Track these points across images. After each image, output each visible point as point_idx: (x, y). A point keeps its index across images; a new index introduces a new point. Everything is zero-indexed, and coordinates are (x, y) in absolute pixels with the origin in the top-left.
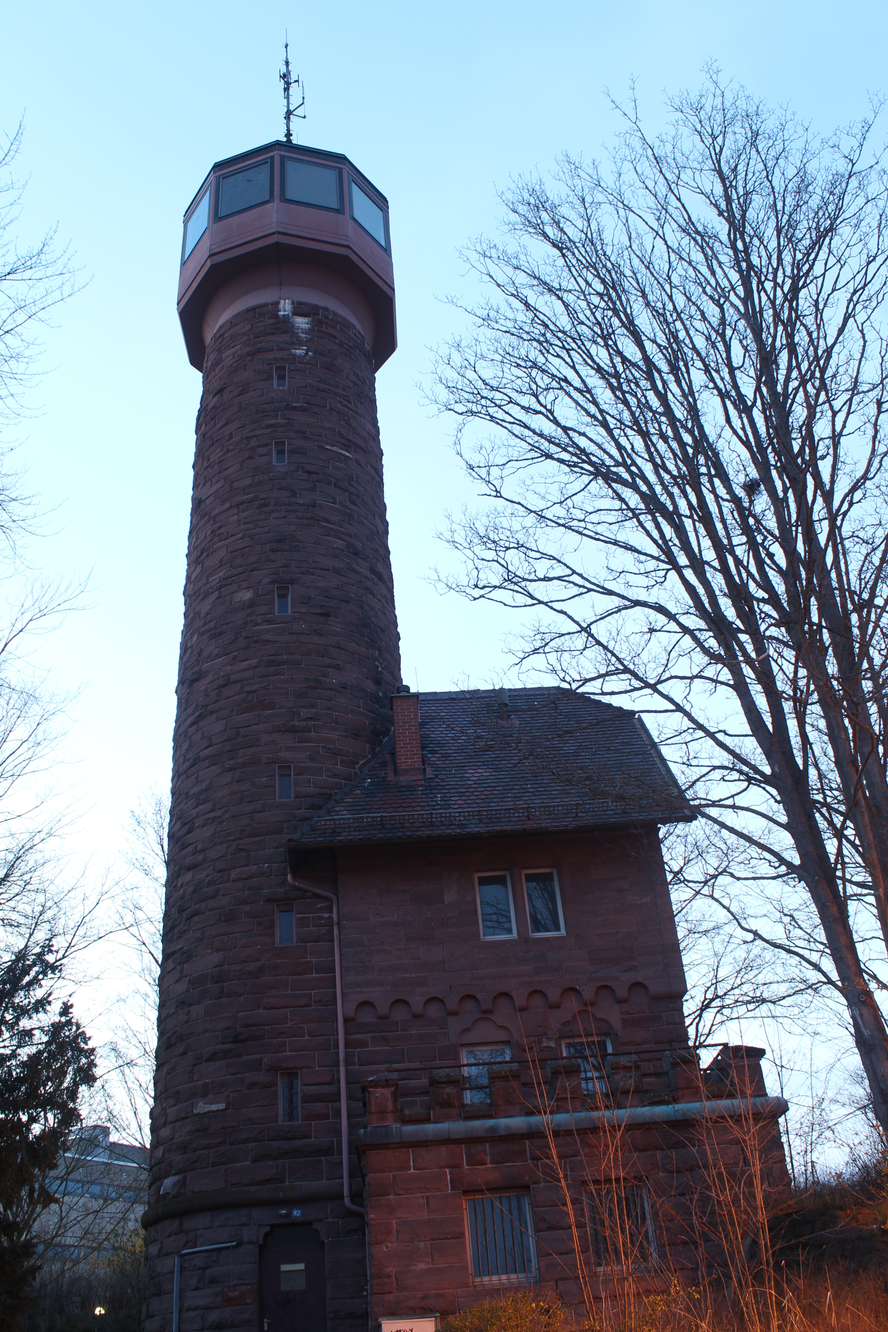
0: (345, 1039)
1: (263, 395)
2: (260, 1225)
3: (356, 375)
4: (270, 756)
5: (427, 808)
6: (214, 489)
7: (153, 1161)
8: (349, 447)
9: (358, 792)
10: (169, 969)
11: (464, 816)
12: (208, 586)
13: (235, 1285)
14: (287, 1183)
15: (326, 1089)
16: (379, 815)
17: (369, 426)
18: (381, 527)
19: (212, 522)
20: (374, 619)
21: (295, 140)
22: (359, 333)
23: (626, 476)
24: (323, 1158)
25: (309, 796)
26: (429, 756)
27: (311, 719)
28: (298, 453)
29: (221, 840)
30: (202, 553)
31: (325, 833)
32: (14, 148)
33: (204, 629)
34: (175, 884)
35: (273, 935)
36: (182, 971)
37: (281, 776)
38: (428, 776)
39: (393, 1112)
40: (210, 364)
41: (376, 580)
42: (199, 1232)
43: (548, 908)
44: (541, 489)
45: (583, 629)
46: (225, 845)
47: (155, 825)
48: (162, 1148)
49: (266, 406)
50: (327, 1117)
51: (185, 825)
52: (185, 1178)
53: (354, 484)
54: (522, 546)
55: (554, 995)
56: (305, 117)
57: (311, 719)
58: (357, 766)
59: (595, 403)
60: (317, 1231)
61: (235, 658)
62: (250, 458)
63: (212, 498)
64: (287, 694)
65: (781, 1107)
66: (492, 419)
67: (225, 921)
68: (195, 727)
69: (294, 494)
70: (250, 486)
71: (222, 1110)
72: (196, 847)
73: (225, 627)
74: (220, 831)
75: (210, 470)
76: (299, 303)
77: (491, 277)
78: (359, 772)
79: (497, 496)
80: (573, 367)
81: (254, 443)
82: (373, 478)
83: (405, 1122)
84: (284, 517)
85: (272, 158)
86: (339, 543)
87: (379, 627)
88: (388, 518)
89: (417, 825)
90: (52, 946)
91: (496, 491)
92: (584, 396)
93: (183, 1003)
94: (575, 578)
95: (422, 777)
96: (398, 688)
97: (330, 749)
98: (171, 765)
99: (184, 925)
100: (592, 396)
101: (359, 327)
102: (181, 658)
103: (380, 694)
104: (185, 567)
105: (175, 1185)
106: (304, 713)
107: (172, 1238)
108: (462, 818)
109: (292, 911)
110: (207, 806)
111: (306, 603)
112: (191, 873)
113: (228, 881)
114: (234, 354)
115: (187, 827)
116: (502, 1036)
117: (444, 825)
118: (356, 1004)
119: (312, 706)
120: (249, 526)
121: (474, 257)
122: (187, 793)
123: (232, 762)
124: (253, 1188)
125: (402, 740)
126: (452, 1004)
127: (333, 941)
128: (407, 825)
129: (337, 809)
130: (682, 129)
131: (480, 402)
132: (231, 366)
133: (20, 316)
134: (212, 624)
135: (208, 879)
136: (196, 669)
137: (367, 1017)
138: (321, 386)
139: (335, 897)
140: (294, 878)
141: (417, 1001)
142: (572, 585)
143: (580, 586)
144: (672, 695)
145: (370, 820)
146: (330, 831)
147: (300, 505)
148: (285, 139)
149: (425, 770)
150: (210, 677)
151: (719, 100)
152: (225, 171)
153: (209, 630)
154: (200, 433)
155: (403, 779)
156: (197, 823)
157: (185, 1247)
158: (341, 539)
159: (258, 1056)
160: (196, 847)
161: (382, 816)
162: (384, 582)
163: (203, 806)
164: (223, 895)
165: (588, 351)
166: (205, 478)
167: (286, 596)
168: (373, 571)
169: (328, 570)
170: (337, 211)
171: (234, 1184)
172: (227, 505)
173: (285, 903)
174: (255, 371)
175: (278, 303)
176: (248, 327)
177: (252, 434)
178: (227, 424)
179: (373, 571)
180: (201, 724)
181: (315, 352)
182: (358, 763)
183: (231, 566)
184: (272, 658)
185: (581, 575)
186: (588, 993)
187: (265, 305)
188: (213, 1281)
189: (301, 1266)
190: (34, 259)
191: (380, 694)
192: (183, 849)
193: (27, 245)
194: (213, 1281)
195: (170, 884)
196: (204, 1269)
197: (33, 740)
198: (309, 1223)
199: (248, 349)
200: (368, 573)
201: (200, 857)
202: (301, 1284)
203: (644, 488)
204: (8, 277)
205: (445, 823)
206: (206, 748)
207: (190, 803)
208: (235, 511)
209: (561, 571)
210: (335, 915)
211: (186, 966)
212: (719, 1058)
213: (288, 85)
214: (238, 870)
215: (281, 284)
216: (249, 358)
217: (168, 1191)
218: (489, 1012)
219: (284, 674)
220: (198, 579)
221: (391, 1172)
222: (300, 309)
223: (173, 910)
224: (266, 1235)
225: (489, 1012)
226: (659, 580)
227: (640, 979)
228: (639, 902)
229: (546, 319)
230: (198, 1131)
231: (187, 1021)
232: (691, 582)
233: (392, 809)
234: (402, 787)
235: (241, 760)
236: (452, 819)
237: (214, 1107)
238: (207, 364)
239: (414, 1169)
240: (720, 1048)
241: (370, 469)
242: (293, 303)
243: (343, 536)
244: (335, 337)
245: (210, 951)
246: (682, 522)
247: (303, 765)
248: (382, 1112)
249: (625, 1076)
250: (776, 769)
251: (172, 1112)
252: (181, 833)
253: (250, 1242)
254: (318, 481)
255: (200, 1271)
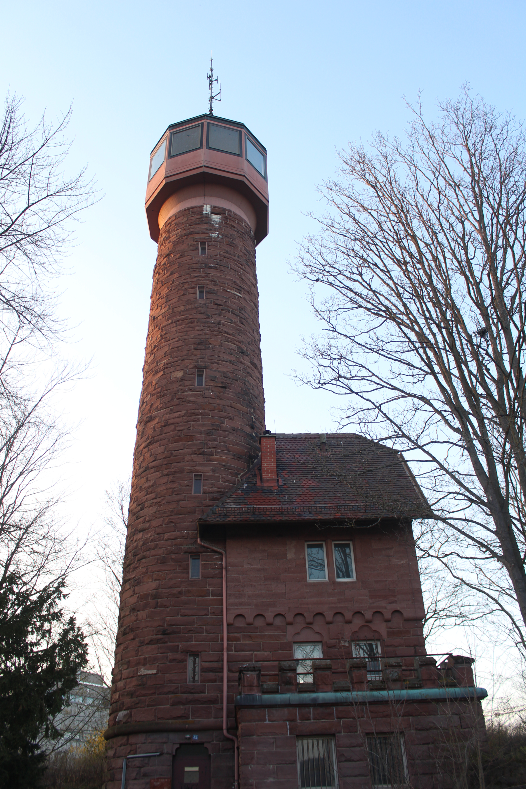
0: (228, 636)
1: (192, 259)
2: (174, 743)
3: (245, 249)
4: (190, 468)
5: (279, 503)
6: (163, 311)
7: (113, 700)
8: (241, 290)
9: (240, 491)
10: (127, 589)
11: (301, 509)
12: (157, 368)
13: (158, 779)
14: (190, 719)
15: (215, 665)
16: (252, 506)
17: (252, 279)
18: (257, 337)
19: (160, 331)
20: (251, 391)
21: (215, 114)
22: (248, 225)
23: (408, 322)
24: (212, 706)
25: (212, 493)
26: (281, 471)
27: (214, 448)
28: (212, 293)
29: (160, 516)
30: (154, 348)
31: (220, 515)
32: (66, 121)
33: (154, 392)
34: (132, 539)
35: (188, 573)
36: (134, 591)
37: (195, 480)
38: (280, 484)
39: (256, 686)
40: (162, 239)
41: (253, 368)
42: (138, 745)
43: (342, 559)
44: (354, 323)
45: (377, 407)
46: (162, 519)
47: (119, 499)
48: (118, 693)
49: (194, 265)
50: (215, 681)
51: (139, 505)
52: (131, 713)
53: (243, 312)
54: (344, 358)
55: (348, 615)
56: (220, 100)
57: (214, 448)
58: (239, 476)
59: (391, 278)
60: (206, 748)
61: (171, 410)
62: (184, 295)
63: (161, 317)
64: (201, 433)
65: (483, 694)
66: (331, 284)
67: (161, 563)
68: (146, 449)
69: (208, 317)
70: (184, 311)
71: (155, 674)
72: (145, 518)
73: (166, 392)
74: (159, 511)
75: (160, 300)
76: (215, 207)
77: (335, 202)
78: (240, 480)
79: (333, 331)
80: (380, 257)
81: (186, 286)
82: (253, 309)
83: (264, 692)
84: (202, 330)
85: (202, 124)
86: (233, 346)
87: (254, 395)
88: (260, 332)
89: (273, 513)
90: (65, 582)
91: (333, 328)
92: (386, 275)
93: (134, 609)
94: (374, 378)
95: (276, 484)
96: (264, 432)
97: (224, 466)
98: (132, 469)
99: (136, 564)
100: (390, 274)
101: (248, 222)
102: (140, 408)
103: (254, 434)
104: (144, 355)
105: (125, 716)
106: (210, 444)
107: (122, 747)
108: (299, 510)
109: (199, 559)
110: (153, 495)
111: (213, 380)
112: (141, 533)
113: (163, 540)
114: (177, 234)
115: (140, 507)
116: (318, 638)
117: (289, 514)
118: (234, 616)
119: (215, 440)
120: (182, 334)
121: (325, 191)
122: (141, 487)
123: (168, 470)
124: (171, 721)
125: (266, 462)
126: (290, 618)
127: (222, 578)
128: (268, 513)
129: (228, 501)
130: (448, 121)
131: (324, 273)
132: (175, 241)
133: (62, 215)
134: (159, 390)
135: (151, 538)
136: (149, 415)
137: (240, 623)
138: (226, 255)
139: (224, 552)
140: (201, 540)
141: (269, 616)
142: (373, 383)
143: (378, 384)
144: (431, 452)
145: (246, 509)
146: (223, 514)
147: (212, 323)
148: (208, 113)
149: (278, 480)
150: (156, 421)
151: (468, 106)
152: (176, 129)
153: (158, 393)
154: (155, 278)
155: (266, 485)
156: (146, 504)
157: (129, 753)
158: (234, 344)
159: (177, 643)
160: (145, 518)
161: (254, 507)
162: (258, 369)
163: (150, 495)
164: (160, 548)
165: (391, 249)
166: (157, 305)
167: (202, 376)
168: (252, 363)
169: (227, 362)
170: (238, 155)
171: (160, 718)
172: (170, 321)
173: (195, 555)
174: (188, 245)
175: (203, 206)
176: (185, 219)
177: (185, 281)
178: (171, 274)
179: (252, 363)
180: (151, 447)
181: (223, 235)
182: (240, 474)
183: (171, 357)
184: (193, 411)
185: (377, 377)
186: (368, 615)
187: (196, 207)
188: (145, 775)
189: (196, 769)
190: (73, 185)
191: (254, 434)
192: (137, 519)
193: (69, 177)
194: (145, 775)
195: (129, 538)
196: (140, 767)
197: (52, 450)
198: (203, 744)
199: (185, 232)
200: (249, 364)
201: (147, 525)
202: (196, 780)
203: (417, 329)
204: (57, 194)
205: (290, 513)
206: (153, 461)
207: (142, 493)
208: (175, 325)
209: (364, 373)
210: (224, 563)
211: (136, 588)
212: (447, 661)
213: (212, 81)
214: (169, 534)
215: (205, 195)
216: (185, 237)
217: (121, 719)
218: (311, 624)
219: (199, 421)
220: (152, 363)
221: (255, 722)
222: (215, 211)
223: (130, 554)
224: (177, 749)
225: (311, 624)
226: (420, 379)
227: (398, 609)
228: (399, 563)
229: (364, 228)
230: (140, 685)
231: (136, 620)
232: (444, 386)
233: (259, 503)
234: (265, 490)
235: (173, 470)
236: (294, 510)
237: (150, 672)
238: (161, 239)
239: (269, 720)
240: (448, 656)
241: (251, 303)
242: (211, 207)
243: (235, 342)
244: (234, 227)
245: (151, 580)
246: (440, 353)
247: (208, 474)
248: (251, 686)
249: (393, 671)
250: (490, 499)
251: (125, 673)
252: (136, 510)
253: (168, 753)
254: (222, 310)
255: (138, 769)
